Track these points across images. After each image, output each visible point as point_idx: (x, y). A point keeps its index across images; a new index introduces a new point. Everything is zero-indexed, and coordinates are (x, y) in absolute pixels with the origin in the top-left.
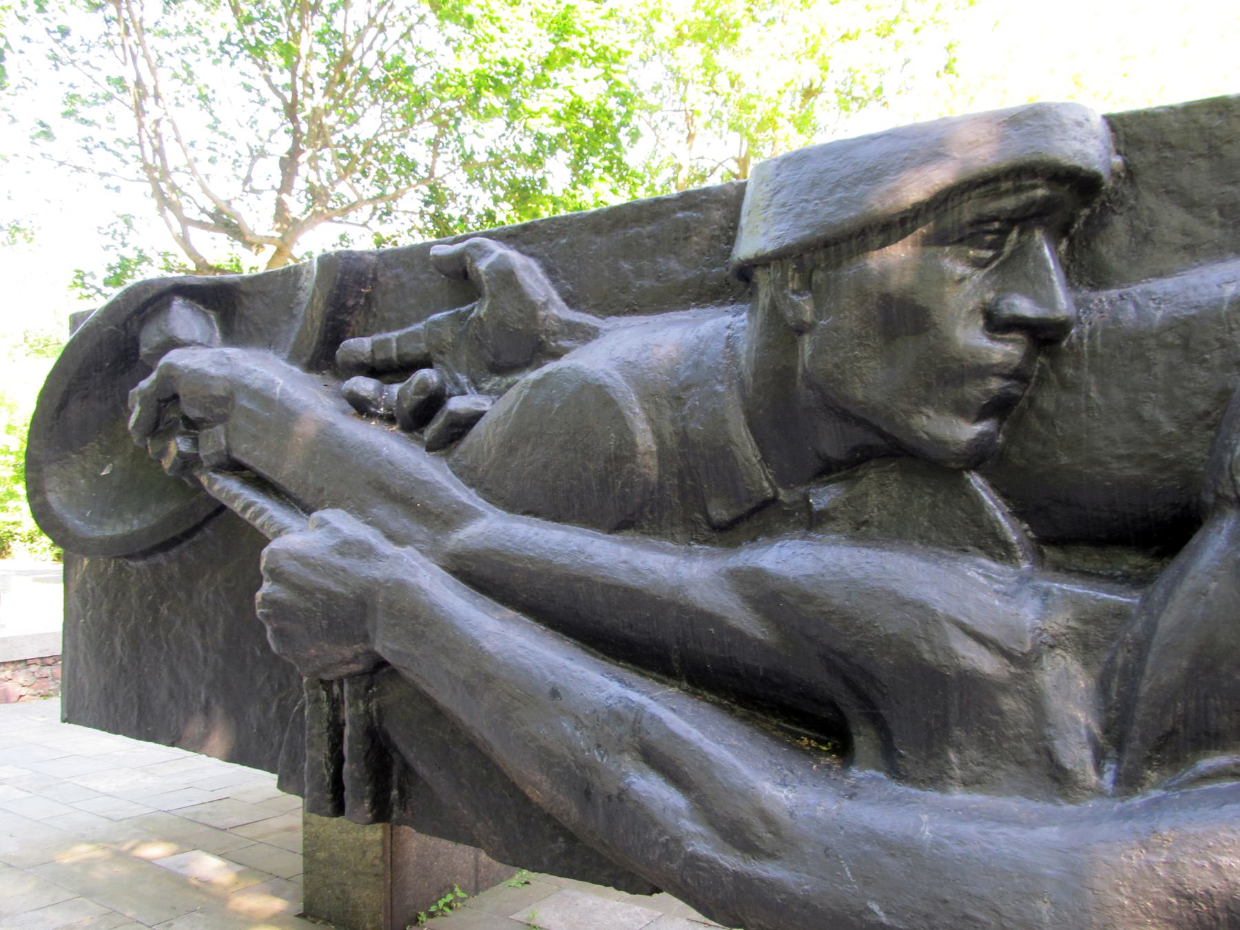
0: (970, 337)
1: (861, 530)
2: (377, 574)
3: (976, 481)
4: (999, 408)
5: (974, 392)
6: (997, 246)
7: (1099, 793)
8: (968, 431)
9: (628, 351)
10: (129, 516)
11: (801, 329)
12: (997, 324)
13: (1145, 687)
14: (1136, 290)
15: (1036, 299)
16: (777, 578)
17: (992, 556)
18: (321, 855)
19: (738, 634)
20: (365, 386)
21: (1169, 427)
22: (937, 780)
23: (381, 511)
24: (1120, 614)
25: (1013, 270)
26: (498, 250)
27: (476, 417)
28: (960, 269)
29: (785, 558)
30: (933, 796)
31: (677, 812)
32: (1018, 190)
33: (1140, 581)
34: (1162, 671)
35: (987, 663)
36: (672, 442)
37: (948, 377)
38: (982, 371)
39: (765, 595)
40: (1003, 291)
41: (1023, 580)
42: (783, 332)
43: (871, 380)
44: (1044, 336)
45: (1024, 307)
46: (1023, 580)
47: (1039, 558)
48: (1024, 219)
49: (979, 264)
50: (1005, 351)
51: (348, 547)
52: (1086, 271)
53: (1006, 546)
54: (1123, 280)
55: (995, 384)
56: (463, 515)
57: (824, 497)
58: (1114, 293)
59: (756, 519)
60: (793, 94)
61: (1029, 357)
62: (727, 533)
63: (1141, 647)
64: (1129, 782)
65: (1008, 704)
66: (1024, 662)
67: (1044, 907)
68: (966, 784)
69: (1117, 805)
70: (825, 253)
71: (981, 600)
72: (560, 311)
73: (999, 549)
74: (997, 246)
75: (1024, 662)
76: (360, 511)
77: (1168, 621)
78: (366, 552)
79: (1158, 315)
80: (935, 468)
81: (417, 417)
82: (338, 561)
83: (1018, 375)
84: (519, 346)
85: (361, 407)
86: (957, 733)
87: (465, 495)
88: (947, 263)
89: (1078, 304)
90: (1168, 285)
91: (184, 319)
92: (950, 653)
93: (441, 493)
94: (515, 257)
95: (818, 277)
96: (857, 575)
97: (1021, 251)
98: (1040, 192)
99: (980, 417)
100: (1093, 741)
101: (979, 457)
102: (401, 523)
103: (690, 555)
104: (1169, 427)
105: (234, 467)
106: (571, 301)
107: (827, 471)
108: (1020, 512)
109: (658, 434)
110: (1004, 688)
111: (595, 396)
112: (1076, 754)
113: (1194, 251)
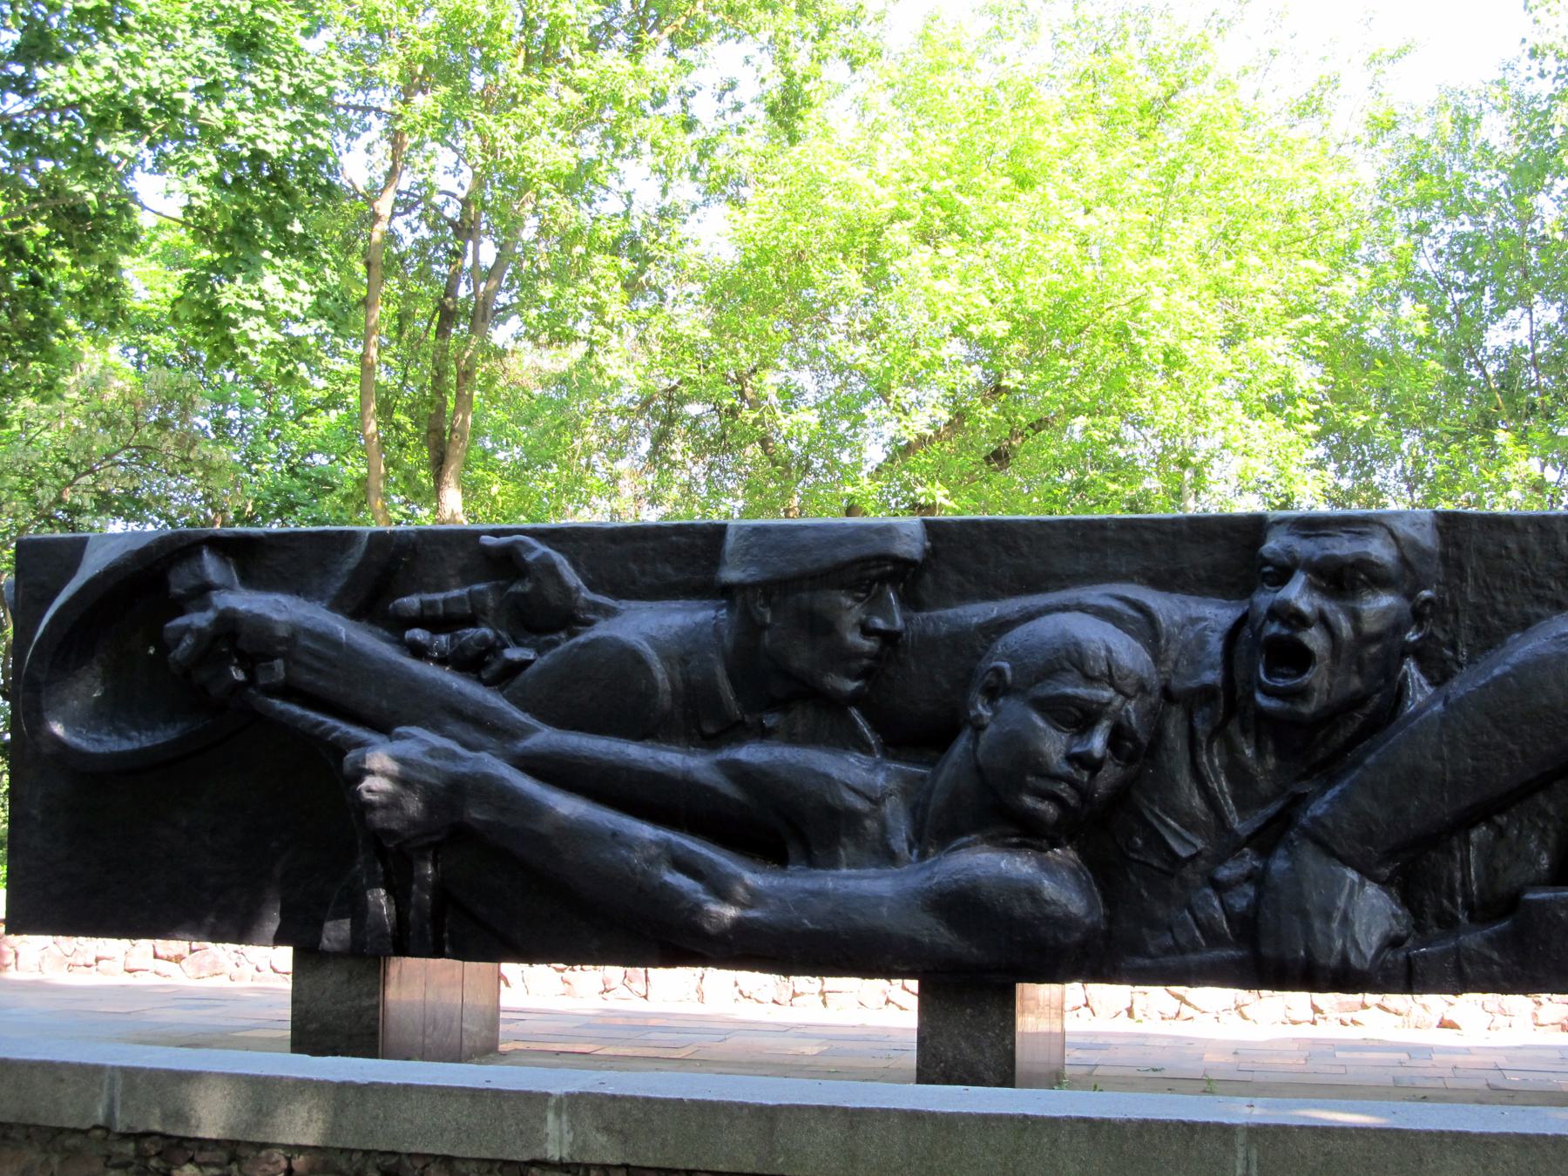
0: (854, 638)
1: (792, 739)
2: (463, 770)
3: (854, 712)
4: (865, 674)
5: (854, 665)
6: (868, 591)
7: (910, 862)
8: (851, 686)
9: (645, 625)
10: (134, 734)
11: (764, 627)
12: (867, 631)
13: (931, 809)
14: (934, 614)
15: (886, 620)
16: (748, 764)
17: (863, 752)
18: (313, 1026)
19: (725, 797)
20: (419, 634)
21: (947, 686)
22: (833, 864)
23: (455, 728)
24: (923, 778)
25: (876, 604)
26: (542, 548)
27: (526, 664)
28: (849, 603)
29: (750, 754)
30: (833, 872)
31: (696, 892)
32: (879, 566)
33: (931, 764)
34: (938, 800)
35: (861, 805)
36: (680, 686)
37: (843, 658)
38: (859, 655)
39: (739, 773)
40: (869, 614)
41: (877, 763)
42: (750, 628)
43: (801, 657)
44: (889, 638)
45: (879, 623)
46: (877, 763)
47: (886, 754)
48: (884, 579)
49: (858, 600)
50: (868, 645)
51: (433, 752)
52: (911, 602)
53: (869, 746)
54: (930, 608)
55: (865, 662)
56: (527, 731)
57: (770, 720)
58: (924, 614)
59: (733, 732)
60: (594, 295)
61: (882, 648)
62: (710, 742)
63: (930, 792)
64: (923, 856)
65: (868, 823)
66: (877, 802)
67: (884, 910)
68: (849, 866)
69: (918, 866)
70: (775, 589)
71: (855, 772)
72: (586, 594)
73: (865, 748)
74: (868, 591)
75: (877, 802)
76: (436, 727)
77: (942, 779)
78: (453, 756)
79: (944, 628)
80: (834, 705)
81: (469, 663)
82: (428, 761)
83: (875, 657)
84: (545, 616)
85: (418, 651)
86: (844, 840)
87: (533, 722)
88: (843, 599)
89: (905, 620)
90: (950, 612)
91: (211, 566)
92: (842, 799)
93: (317, 732)
94: (557, 557)
95: (775, 599)
96: (793, 761)
97: (880, 593)
98: (889, 568)
99: (856, 679)
100: (908, 840)
101: (856, 699)
102: (475, 736)
103: (692, 754)
104: (947, 686)
105: (289, 692)
106: (592, 587)
107: (773, 705)
108: (876, 729)
109: (672, 681)
110: (866, 815)
111: (628, 659)
112: (900, 843)
113: (964, 597)
